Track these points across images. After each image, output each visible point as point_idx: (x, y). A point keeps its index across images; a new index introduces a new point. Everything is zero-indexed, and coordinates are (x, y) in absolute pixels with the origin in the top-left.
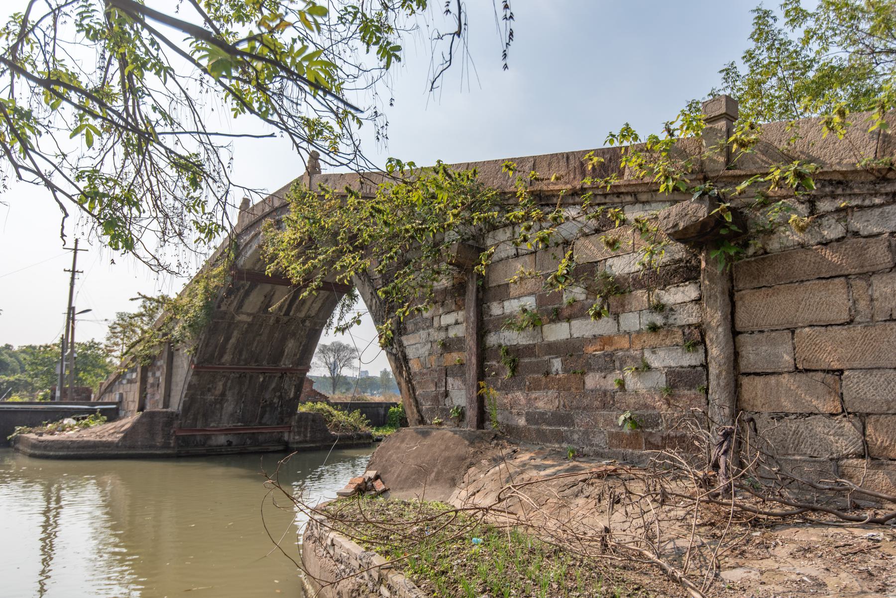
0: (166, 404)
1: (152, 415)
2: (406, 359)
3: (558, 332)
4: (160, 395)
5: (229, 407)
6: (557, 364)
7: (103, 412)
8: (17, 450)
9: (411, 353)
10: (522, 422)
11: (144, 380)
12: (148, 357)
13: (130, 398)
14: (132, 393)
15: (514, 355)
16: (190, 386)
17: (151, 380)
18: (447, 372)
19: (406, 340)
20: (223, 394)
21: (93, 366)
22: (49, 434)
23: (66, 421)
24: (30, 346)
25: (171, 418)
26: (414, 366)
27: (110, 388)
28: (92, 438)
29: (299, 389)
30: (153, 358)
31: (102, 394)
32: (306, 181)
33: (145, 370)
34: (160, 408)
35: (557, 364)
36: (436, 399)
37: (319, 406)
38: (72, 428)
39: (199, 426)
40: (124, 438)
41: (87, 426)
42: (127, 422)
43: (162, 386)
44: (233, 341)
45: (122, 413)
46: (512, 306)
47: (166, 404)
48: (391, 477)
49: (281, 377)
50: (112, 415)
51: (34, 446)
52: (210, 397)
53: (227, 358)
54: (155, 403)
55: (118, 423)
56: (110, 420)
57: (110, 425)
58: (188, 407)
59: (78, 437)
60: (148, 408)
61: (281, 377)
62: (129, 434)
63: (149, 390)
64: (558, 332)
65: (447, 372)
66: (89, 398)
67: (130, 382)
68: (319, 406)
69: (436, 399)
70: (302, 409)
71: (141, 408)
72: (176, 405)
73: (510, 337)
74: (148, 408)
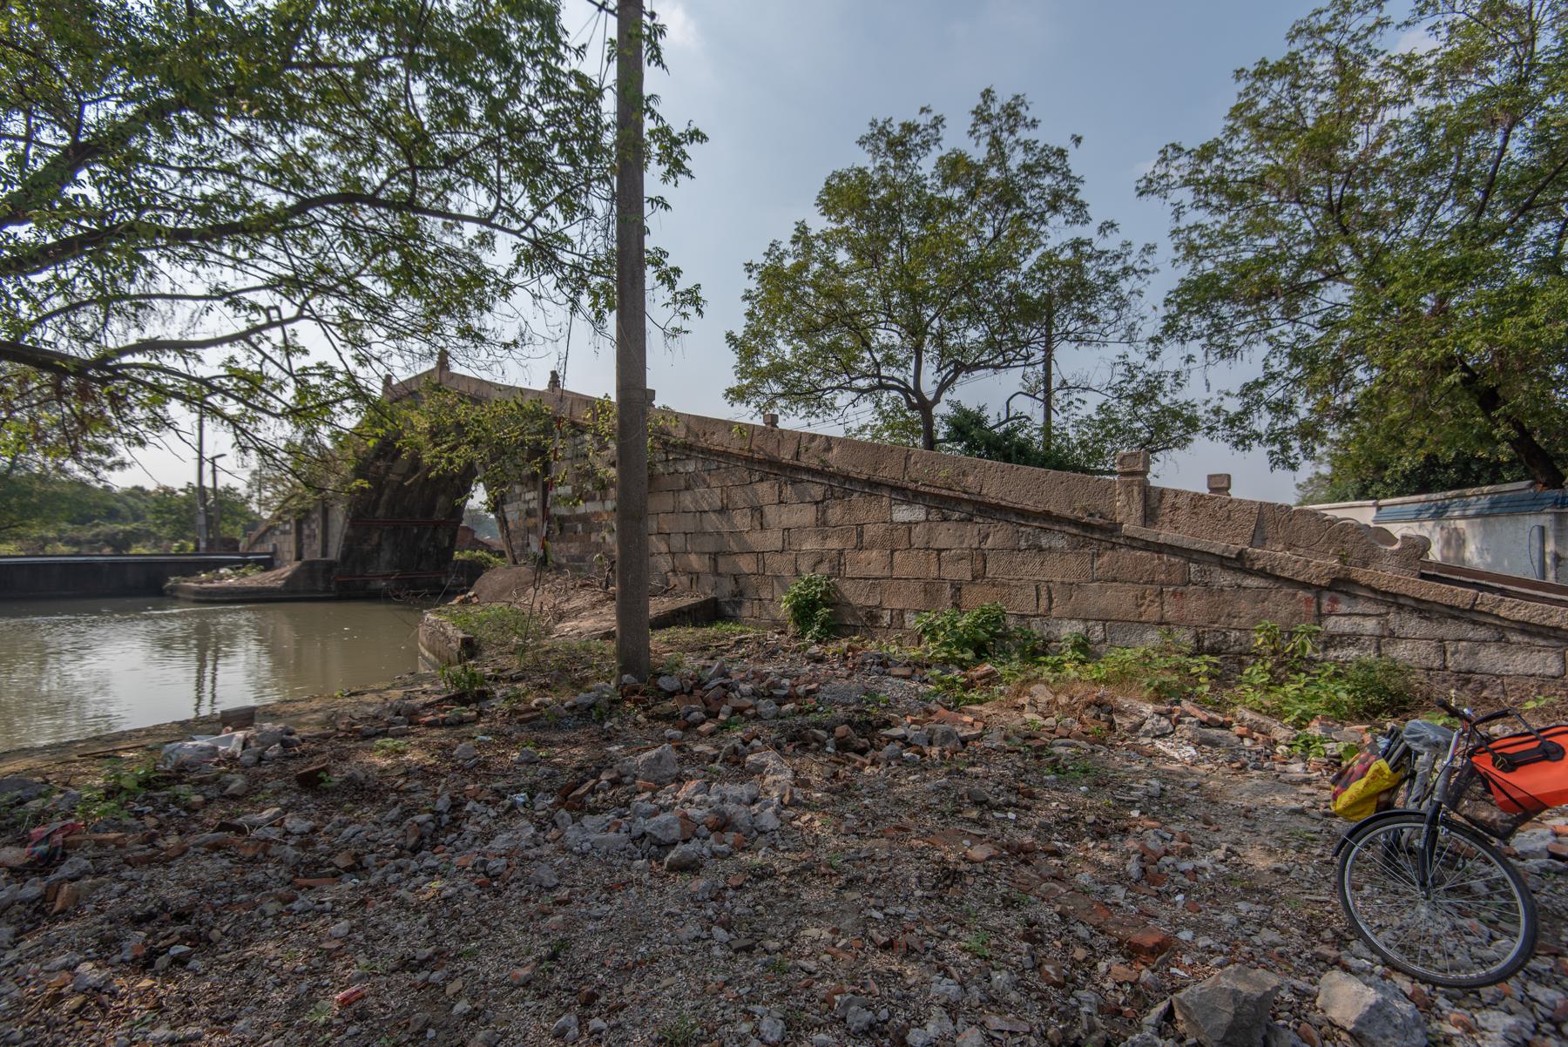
0: (325, 554)
1: (311, 564)
2: (506, 522)
3: (583, 508)
4: (317, 545)
5: (386, 555)
6: (580, 527)
7: (258, 562)
8: (176, 598)
9: (509, 517)
10: (564, 561)
11: (299, 531)
12: (302, 510)
13: (286, 548)
14: (288, 545)
15: (562, 520)
16: (347, 538)
17: (306, 532)
18: (528, 530)
19: (507, 508)
20: (379, 544)
21: (232, 514)
22: (204, 581)
23: (222, 571)
24: (136, 488)
25: (331, 565)
26: (511, 526)
27: (261, 538)
28: (255, 584)
29: (453, 538)
30: (307, 512)
31: (253, 545)
32: (437, 375)
33: (299, 523)
34: (318, 557)
35: (580, 527)
36: (522, 548)
37: (478, 553)
38: (230, 577)
39: (358, 572)
40: (286, 585)
41: (245, 575)
42: (287, 570)
43: (319, 537)
44: (385, 498)
45: (277, 563)
46: (561, 490)
47: (325, 554)
48: (483, 595)
49: (435, 529)
50: (268, 564)
51: (197, 593)
52: (366, 547)
53: (380, 512)
54: (313, 552)
55: (277, 572)
56: (266, 570)
57: (270, 574)
58: (346, 556)
59: (34, 627)
60: (306, 558)
61: (435, 529)
62: (290, 581)
63: (306, 541)
64: (583, 508)
65: (528, 530)
66: (237, 548)
67: (284, 533)
68: (478, 553)
69: (522, 548)
70: (457, 555)
71: (299, 558)
72: (334, 553)
73: (562, 510)
74: (306, 558)
